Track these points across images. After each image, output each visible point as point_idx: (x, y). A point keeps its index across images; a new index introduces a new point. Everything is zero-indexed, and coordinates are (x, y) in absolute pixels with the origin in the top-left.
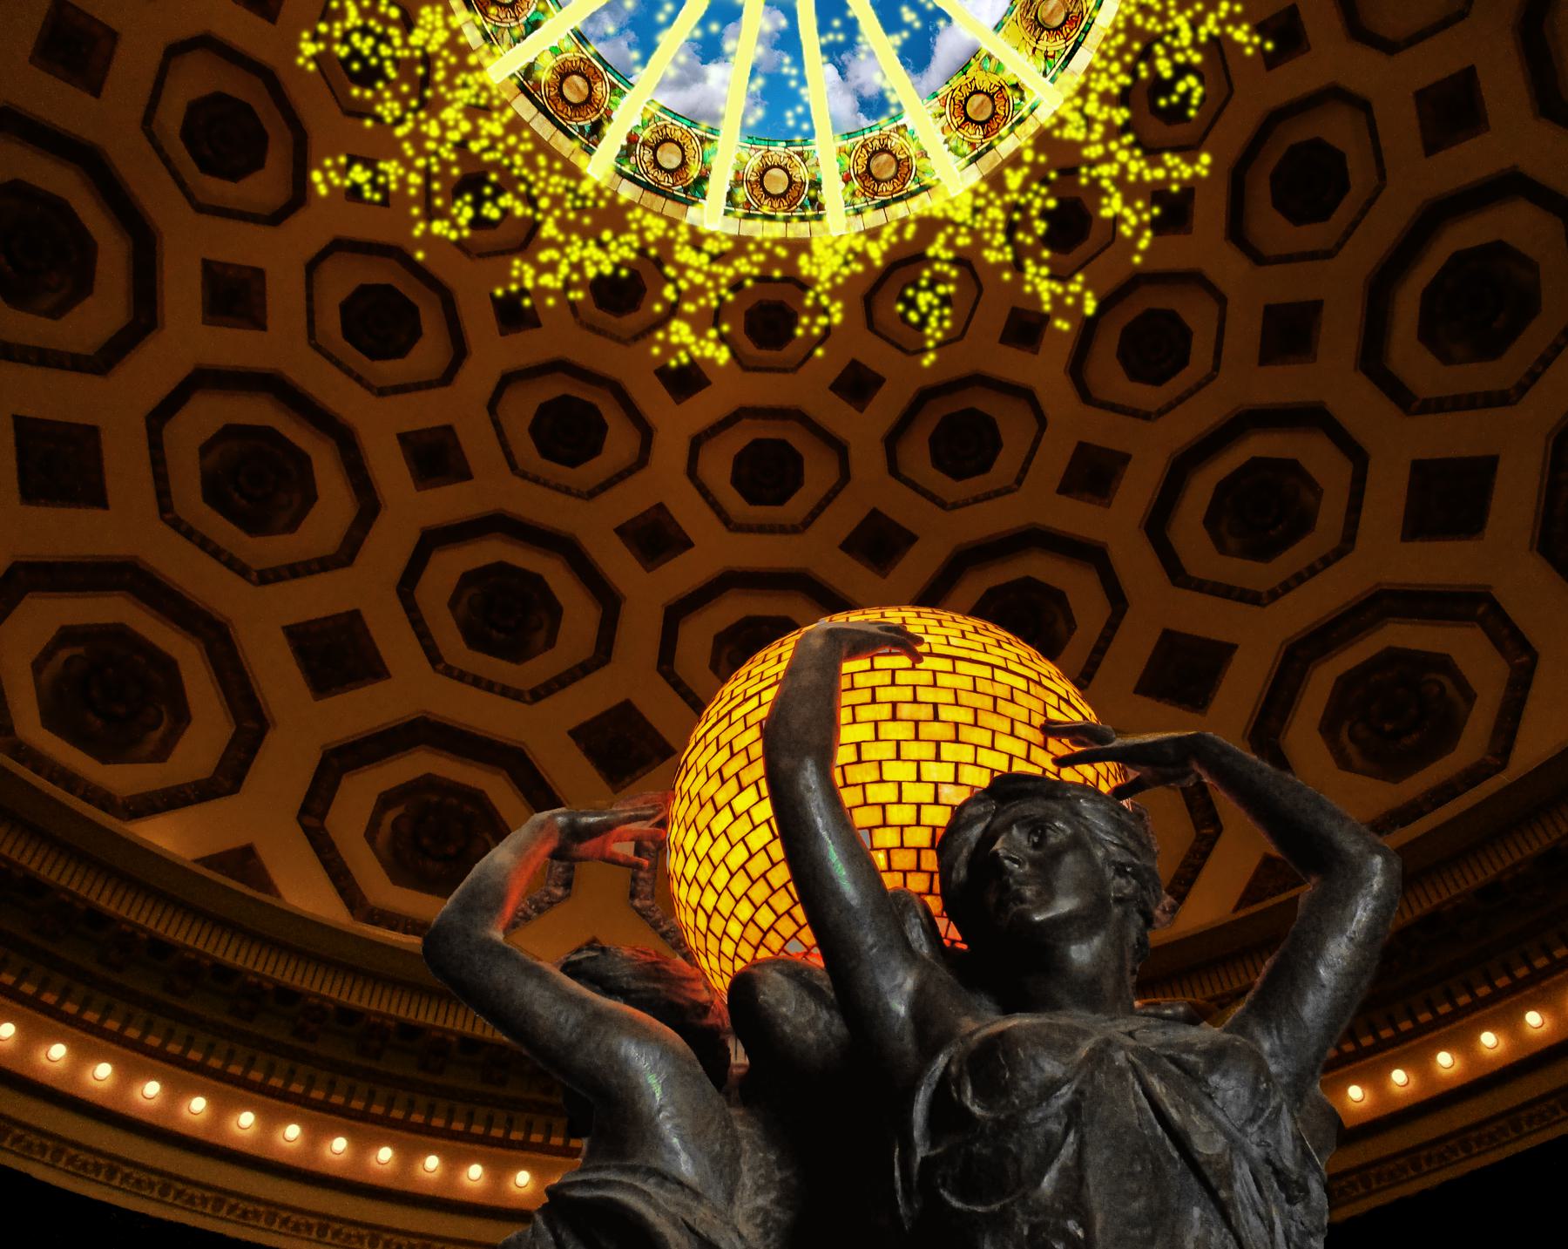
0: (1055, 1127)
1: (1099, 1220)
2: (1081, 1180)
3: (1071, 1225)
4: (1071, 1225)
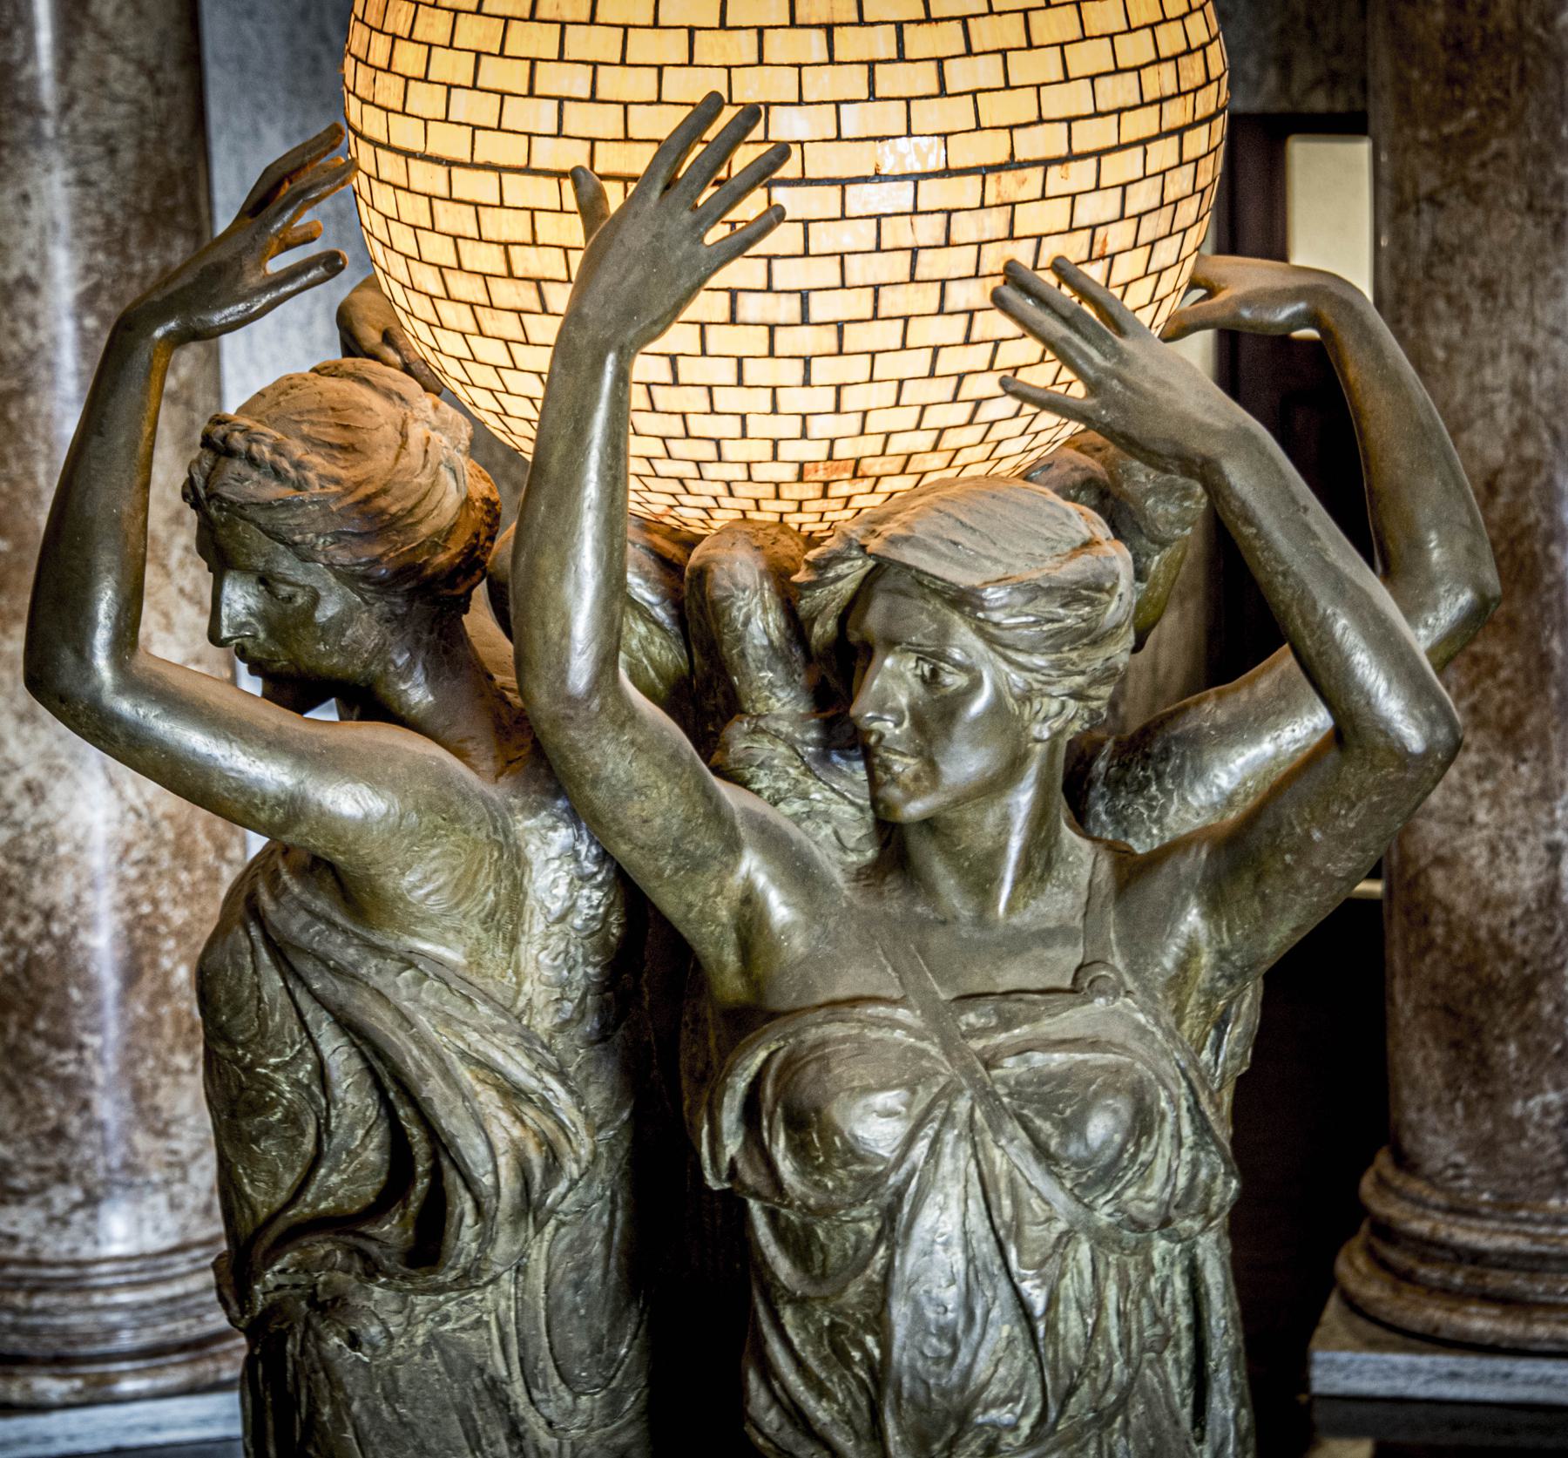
0: (869, 1229)
1: (900, 1332)
2: (885, 1304)
3: (870, 1340)
4: (870, 1340)
